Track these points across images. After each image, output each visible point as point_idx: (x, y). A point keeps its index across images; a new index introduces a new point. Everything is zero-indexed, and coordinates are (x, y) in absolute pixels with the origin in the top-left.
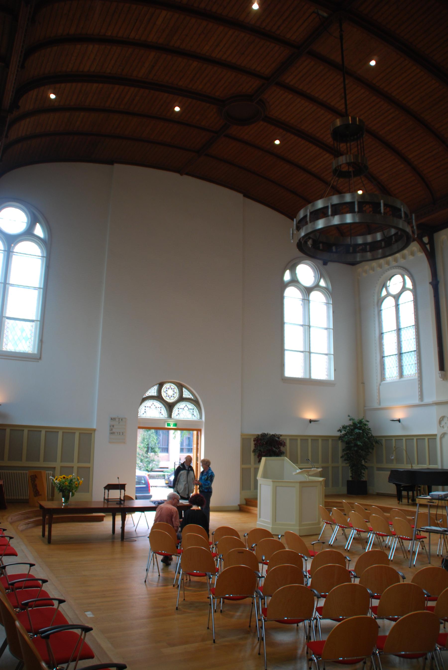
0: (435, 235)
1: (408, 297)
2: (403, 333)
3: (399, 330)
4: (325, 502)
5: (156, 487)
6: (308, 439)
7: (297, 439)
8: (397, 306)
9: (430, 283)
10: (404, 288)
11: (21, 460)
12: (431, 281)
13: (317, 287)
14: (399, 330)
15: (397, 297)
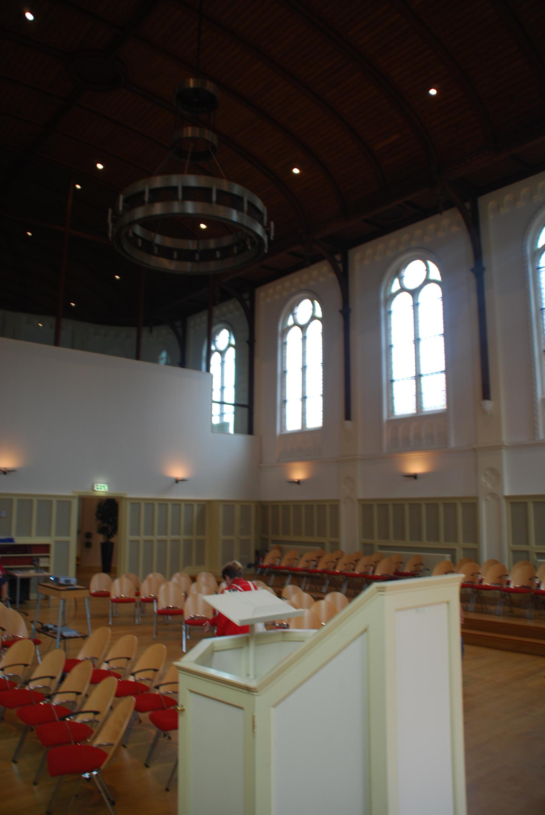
0: (351, 252)
3: (418, 377)
6: (526, 503)
7: (387, 505)
10: (313, 318)
11: (68, 543)
13: (296, 324)
14: (418, 377)
15: (304, 328)
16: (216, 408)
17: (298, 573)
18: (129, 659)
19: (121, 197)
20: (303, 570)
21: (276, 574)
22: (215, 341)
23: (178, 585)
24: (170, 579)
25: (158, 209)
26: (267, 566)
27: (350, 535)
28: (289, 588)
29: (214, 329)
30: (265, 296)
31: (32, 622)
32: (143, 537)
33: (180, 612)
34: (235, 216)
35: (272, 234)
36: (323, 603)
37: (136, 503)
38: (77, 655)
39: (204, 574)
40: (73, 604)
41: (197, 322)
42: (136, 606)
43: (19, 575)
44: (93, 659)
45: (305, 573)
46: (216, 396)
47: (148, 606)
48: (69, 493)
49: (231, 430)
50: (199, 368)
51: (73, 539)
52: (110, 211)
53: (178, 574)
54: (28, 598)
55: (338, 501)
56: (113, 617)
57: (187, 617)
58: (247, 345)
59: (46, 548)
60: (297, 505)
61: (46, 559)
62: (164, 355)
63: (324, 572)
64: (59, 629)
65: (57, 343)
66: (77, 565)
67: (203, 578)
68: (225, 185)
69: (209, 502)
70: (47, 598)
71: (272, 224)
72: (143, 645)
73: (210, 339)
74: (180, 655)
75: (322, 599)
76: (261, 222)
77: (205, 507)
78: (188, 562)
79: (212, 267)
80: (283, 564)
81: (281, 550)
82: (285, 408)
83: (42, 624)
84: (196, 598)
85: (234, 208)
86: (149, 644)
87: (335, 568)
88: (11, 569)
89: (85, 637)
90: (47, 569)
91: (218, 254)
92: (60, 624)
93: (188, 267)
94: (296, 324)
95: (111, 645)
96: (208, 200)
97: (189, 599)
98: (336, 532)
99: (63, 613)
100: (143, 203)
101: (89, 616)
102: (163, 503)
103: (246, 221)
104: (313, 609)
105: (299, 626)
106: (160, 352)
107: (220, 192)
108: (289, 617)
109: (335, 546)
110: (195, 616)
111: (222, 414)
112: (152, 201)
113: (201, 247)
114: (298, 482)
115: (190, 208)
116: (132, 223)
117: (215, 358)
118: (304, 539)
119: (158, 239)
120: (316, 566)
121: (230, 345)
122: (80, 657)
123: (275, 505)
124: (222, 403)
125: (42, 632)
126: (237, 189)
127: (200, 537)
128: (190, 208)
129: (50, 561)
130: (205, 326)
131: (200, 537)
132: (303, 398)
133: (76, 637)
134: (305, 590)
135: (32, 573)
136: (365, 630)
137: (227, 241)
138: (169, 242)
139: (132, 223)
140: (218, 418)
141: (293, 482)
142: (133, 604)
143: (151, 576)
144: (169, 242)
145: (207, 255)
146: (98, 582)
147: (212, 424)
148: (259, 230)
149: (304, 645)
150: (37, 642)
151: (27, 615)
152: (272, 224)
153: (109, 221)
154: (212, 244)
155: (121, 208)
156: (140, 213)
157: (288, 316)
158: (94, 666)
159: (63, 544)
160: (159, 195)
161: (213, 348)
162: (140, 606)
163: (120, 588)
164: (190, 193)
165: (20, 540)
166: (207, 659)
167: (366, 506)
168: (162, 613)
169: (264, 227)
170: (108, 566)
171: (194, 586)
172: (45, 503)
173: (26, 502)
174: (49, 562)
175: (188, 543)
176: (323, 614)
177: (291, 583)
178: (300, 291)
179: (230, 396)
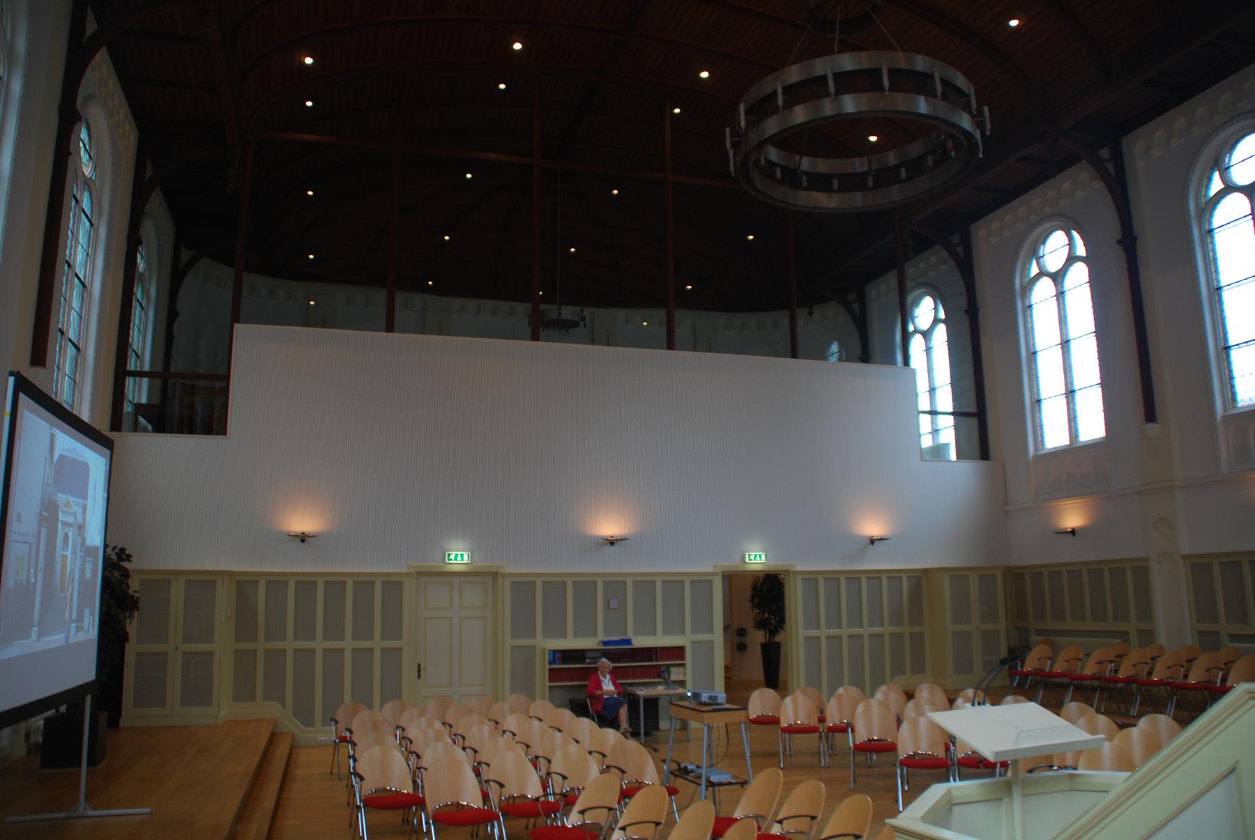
0: (1125, 141)
1: (1080, 273)
2: (1074, 347)
4: (236, 651)
5: (419, 671)
8: (1060, 295)
9: (1118, 242)
10: (1071, 259)
11: (712, 642)
12: (1119, 237)
15: (1058, 277)
16: (925, 422)
17: (1085, 682)
18: (813, 818)
19: (742, 107)
20: (1092, 677)
21: (1047, 686)
22: (913, 319)
23: (884, 705)
24: (872, 695)
25: (800, 114)
26: (1028, 673)
27: (1172, 617)
28: (1072, 706)
29: (909, 299)
30: (988, 235)
31: (664, 761)
32: (824, 632)
33: (892, 748)
34: (922, 106)
35: (988, 126)
36: (1134, 731)
37: (811, 579)
38: (733, 812)
39: (925, 686)
40: (723, 736)
41: (881, 291)
42: (820, 738)
43: (642, 692)
44: (757, 817)
45: (1096, 683)
46: (924, 403)
47: (838, 737)
48: (709, 569)
49: (953, 456)
50: (892, 362)
51: (717, 637)
52: (728, 130)
53: (883, 688)
54: (657, 728)
55: (1147, 559)
56: (784, 755)
57: (902, 755)
58: (965, 318)
59: (679, 652)
60: (1075, 570)
61: (681, 669)
62: (834, 347)
63: (1129, 680)
64: (704, 772)
65: (670, 346)
66: (726, 678)
67: (924, 693)
68: (900, 60)
69: (926, 571)
70: (684, 727)
71: (986, 109)
72: (834, 799)
73: (905, 313)
74: (895, 813)
75: (1134, 726)
76: (967, 108)
77: (921, 580)
78: (898, 669)
79: (896, 194)
80: (1058, 669)
81: (1051, 645)
82: (1040, 411)
83: (679, 764)
84: (915, 724)
85: (920, 94)
86: (844, 796)
87: (1150, 673)
88: (631, 685)
89: (743, 783)
90: (682, 683)
91: (903, 172)
92: (704, 764)
93: (857, 200)
94: (1042, 273)
95: (784, 798)
96: (877, 87)
97: (904, 726)
98: (1146, 612)
99: (709, 746)
100: (776, 111)
101: (748, 754)
102: (854, 578)
103: (943, 110)
104: (1116, 740)
105: (1095, 764)
106: (829, 345)
107: (894, 72)
108: (1079, 751)
109: (1148, 637)
110: (915, 754)
111: (935, 432)
112: (789, 105)
113: (874, 167)
114: (1073, 532)
115: (849, 104)
116: (763, 144)
117: (917, 344)
118: (1089, 625)
119: (806, 164)
120: (1116, 671)
121: (936, 321)
122: (737, 814)
123: (1036, 572)
124: (933, 413)
125: (679, 775)
126: (921, 63)
127: (916, 629)
128: (849, 104)
129: (686, 673)
130: (894, 295)
131: (916, 629)
132: (1069, 395)
133: (730, 784)
134: (1098, 711)
135: (660, 690)
136: (1233, 770)
137: (915, 149)
138: (822, 166)
139: (763, 144)
140: (930, 436)
141: (1065, 532)
142: (816, 735)
143: (841, 690)
144: (822, 166)
145: (885, 177)
146: (760, 702)
147: (921, 450)
148: (966, 122)
149: (1108, 798)
150: (672, 791)
151: (655, 750)
152: (986, 109)
153: (728, 145)
154: (892, 158)
155: (743, 124)
156: (772, 126)
157: (1030, 262)
158: (759, 829)
159: (703, 644)
160: (797, 94)
161: (911, 328)
162: (827, 739)
163: (794, 710)
164: (847, 83)
165: (640, 642)
166: (943, 814)
167: (1199, 567)
168: (860, 748)
169: (973, 116)
170: (773, 678)
171: (910, 705)
172: (674, 584)
173: (645, 585)
174: (685, 674)
175: (897, 639)
176: (1137, 751)
177: (1072, 700)
178: (1044, 219)
179: (945, 401)
